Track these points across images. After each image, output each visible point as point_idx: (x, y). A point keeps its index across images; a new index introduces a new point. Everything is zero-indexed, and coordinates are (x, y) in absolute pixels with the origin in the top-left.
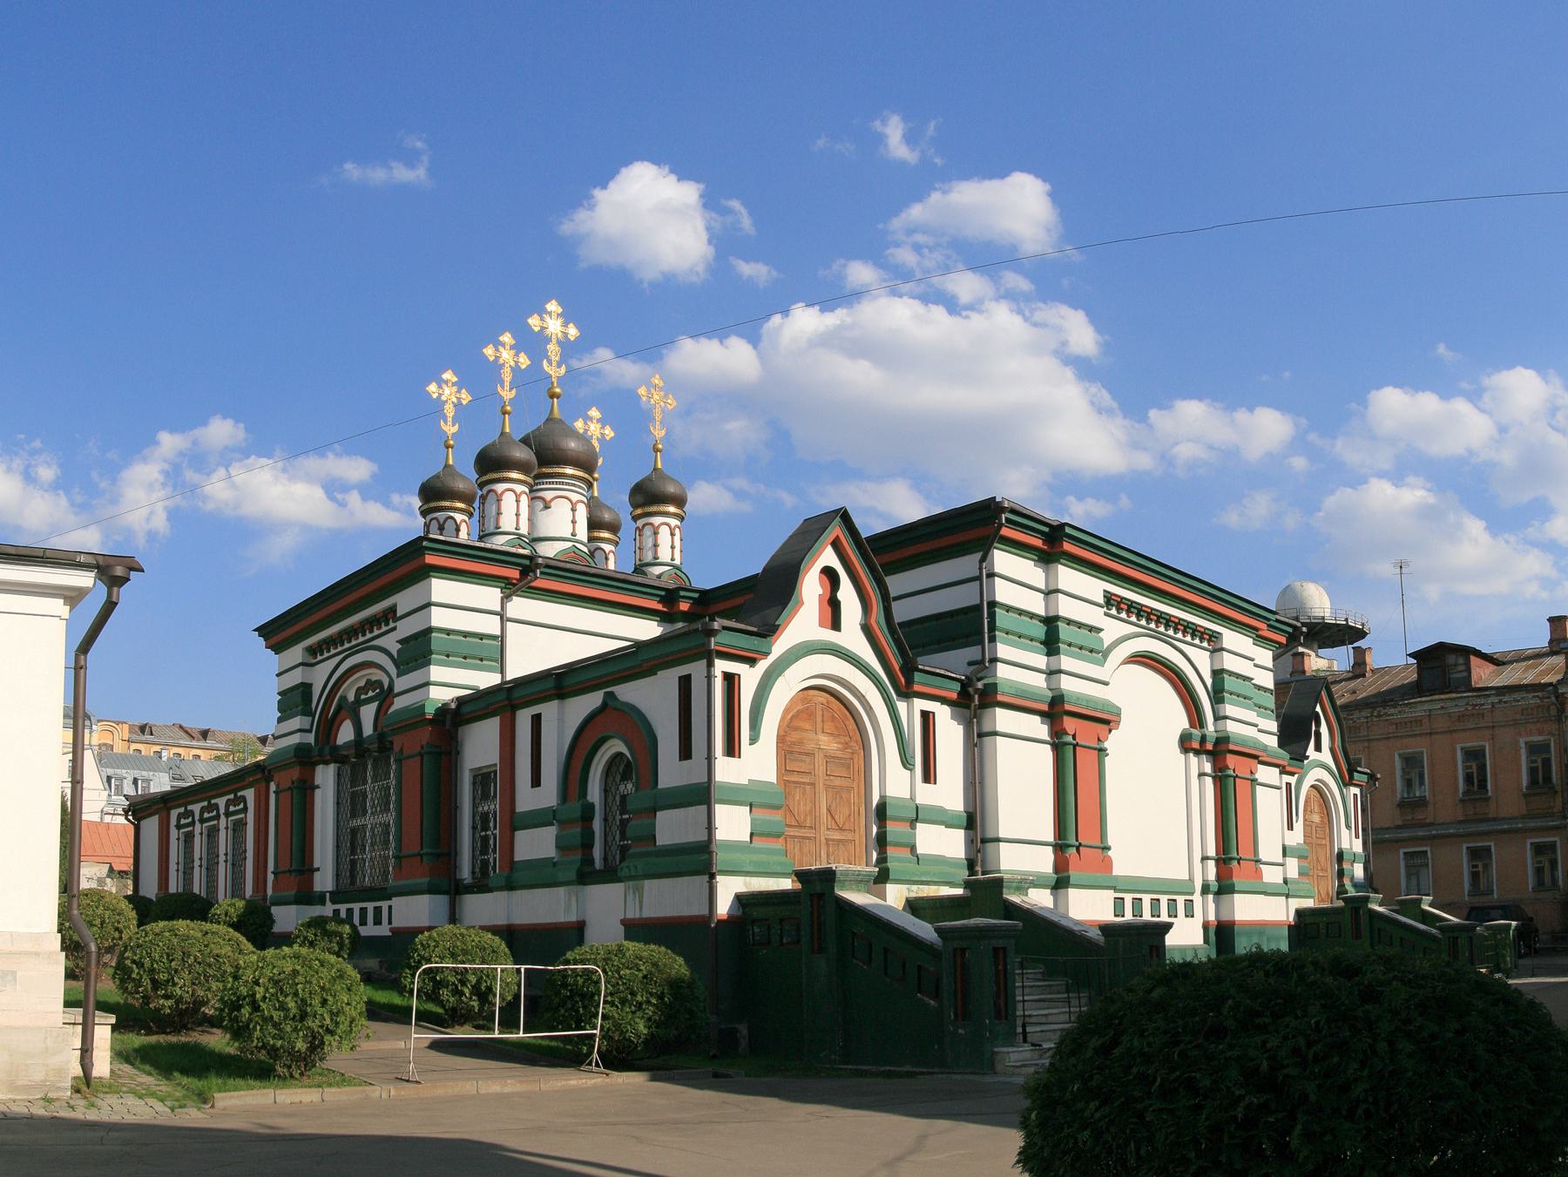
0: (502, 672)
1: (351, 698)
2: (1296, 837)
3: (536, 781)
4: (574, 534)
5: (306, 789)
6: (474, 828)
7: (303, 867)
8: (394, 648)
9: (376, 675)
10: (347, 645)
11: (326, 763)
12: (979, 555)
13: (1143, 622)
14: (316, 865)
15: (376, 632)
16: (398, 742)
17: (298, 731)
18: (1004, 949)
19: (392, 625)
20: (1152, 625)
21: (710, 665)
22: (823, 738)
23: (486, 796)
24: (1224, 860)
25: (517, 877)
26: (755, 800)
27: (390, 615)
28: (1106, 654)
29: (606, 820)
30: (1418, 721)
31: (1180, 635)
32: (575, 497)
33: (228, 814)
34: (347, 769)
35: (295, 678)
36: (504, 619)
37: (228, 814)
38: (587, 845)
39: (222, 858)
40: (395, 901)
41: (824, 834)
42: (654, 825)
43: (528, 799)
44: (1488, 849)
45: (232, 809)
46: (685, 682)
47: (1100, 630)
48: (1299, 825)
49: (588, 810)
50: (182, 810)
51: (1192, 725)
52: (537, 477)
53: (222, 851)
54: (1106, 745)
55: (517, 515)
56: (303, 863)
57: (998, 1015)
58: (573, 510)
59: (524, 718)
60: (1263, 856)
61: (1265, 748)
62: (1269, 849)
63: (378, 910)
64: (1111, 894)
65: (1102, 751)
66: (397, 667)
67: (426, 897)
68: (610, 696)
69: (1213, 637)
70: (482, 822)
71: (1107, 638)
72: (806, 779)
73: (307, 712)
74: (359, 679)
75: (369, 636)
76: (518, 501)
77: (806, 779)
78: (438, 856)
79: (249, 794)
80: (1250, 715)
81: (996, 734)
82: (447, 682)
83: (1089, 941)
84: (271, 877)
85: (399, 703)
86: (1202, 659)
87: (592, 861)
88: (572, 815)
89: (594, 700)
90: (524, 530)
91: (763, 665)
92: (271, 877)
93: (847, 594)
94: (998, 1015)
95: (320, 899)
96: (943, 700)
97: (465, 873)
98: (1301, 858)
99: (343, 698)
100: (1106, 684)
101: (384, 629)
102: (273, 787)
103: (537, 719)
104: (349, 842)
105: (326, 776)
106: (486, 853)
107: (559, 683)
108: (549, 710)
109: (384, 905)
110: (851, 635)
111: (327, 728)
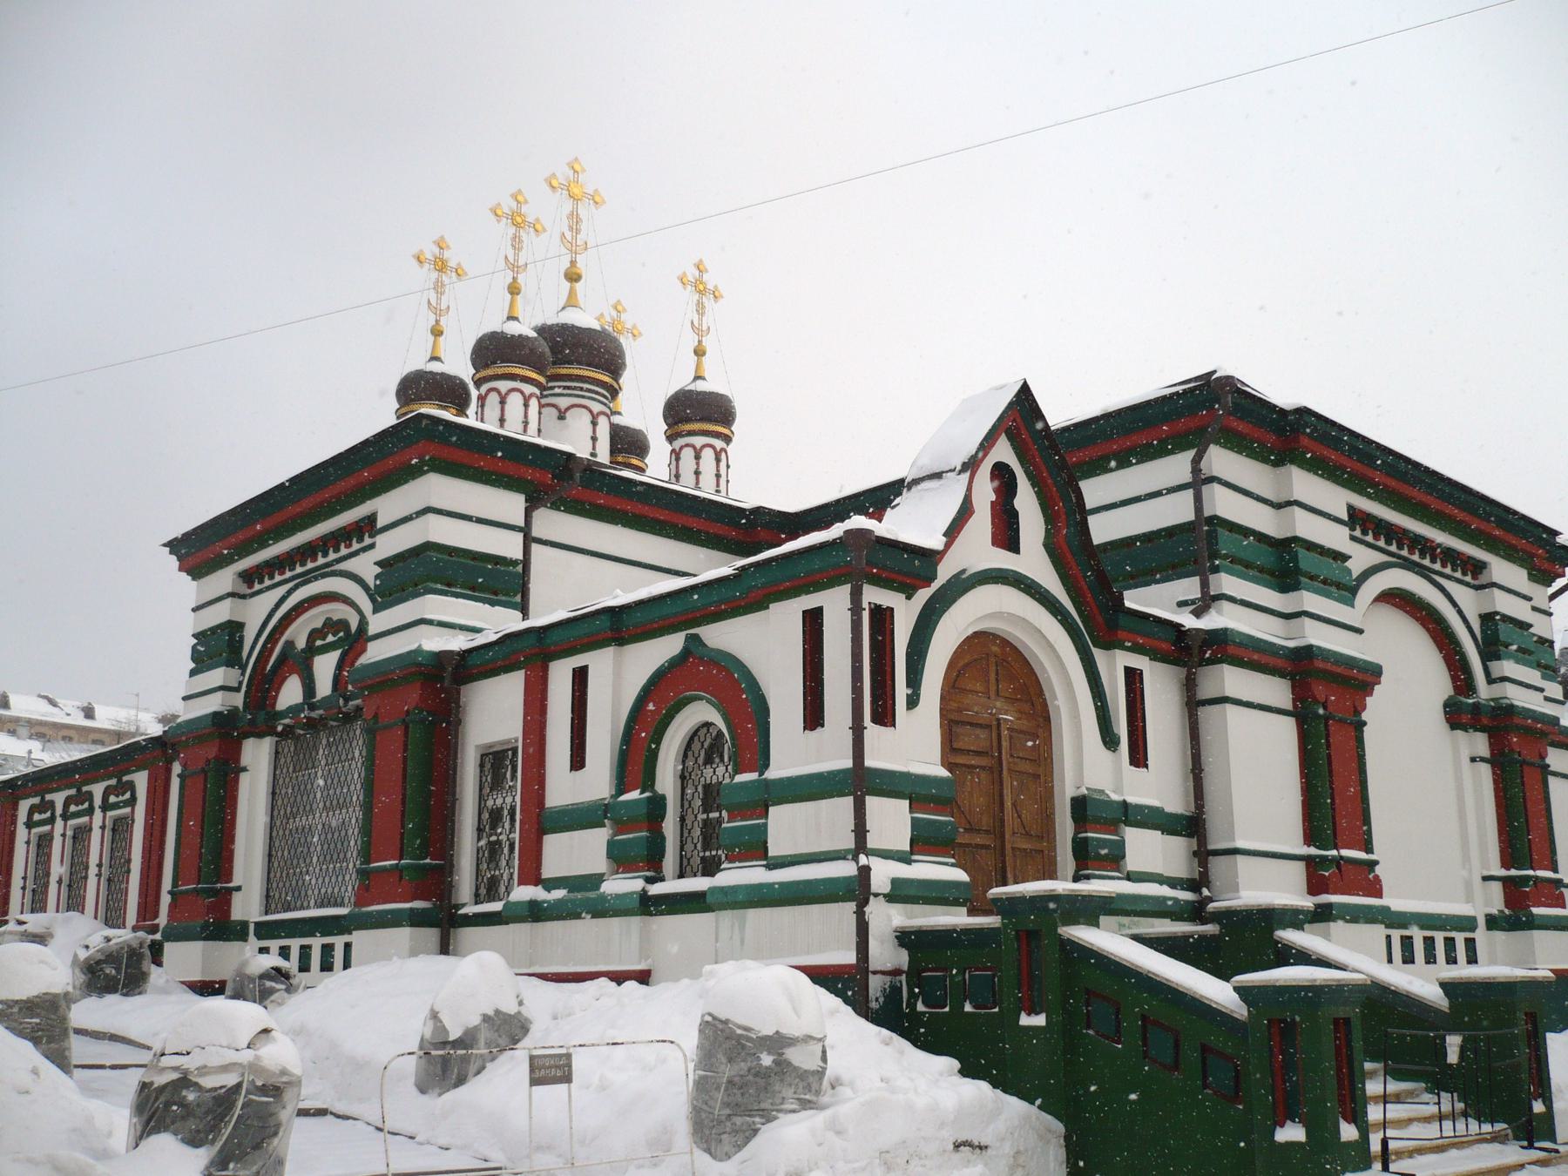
1: (301, 643)
3: (578, 760)
5: (227, 772)
6: (480, 830)
9: (338, 611)
10: (299, 570)
11: (260, 735)
12: (1191, 454)
13: (1393, 548)
15: (344, 551)
17: (217, 694)
27: (368, 526)
28: (1354, 591)
29: (683, 819)
32: (597, 407)
33: (106, 807)
35: (220, 614)
37: (106, 807)
39: (93, 870)
42: (765, 825)
43: (565, 787)
45: (112, 799)
46: (813, 619)
50: (36, 800)
52: (552, 378)
53: (93, 860)
58: (594, 424)
59: (560, 675)
63: (327, 950)
64: (1379, 931)
66: (373, 601)
68: (694, 640)
69: (1477, 567)
70: (491, 819)
71: (1356, 566)
74: (314, 618)
75: (332, 556)
76: (526, 405)
81: (1225, 700)
82: (452, 622)
83: (1437, 1011)
84: (165, 900)
85: (376, 652)
89: (669, 646)
91: (923, 595)
92: (165, 900)
93: (1026, 502)
99: (290, 644)
100: (1360, 631)
102: (177, 768)
103: (580, 676)
105: (257, 755)
107: (618, 626)
108: (600, 663)
109: (339, 941)
110: (1033, 560)
111: (263, 687)
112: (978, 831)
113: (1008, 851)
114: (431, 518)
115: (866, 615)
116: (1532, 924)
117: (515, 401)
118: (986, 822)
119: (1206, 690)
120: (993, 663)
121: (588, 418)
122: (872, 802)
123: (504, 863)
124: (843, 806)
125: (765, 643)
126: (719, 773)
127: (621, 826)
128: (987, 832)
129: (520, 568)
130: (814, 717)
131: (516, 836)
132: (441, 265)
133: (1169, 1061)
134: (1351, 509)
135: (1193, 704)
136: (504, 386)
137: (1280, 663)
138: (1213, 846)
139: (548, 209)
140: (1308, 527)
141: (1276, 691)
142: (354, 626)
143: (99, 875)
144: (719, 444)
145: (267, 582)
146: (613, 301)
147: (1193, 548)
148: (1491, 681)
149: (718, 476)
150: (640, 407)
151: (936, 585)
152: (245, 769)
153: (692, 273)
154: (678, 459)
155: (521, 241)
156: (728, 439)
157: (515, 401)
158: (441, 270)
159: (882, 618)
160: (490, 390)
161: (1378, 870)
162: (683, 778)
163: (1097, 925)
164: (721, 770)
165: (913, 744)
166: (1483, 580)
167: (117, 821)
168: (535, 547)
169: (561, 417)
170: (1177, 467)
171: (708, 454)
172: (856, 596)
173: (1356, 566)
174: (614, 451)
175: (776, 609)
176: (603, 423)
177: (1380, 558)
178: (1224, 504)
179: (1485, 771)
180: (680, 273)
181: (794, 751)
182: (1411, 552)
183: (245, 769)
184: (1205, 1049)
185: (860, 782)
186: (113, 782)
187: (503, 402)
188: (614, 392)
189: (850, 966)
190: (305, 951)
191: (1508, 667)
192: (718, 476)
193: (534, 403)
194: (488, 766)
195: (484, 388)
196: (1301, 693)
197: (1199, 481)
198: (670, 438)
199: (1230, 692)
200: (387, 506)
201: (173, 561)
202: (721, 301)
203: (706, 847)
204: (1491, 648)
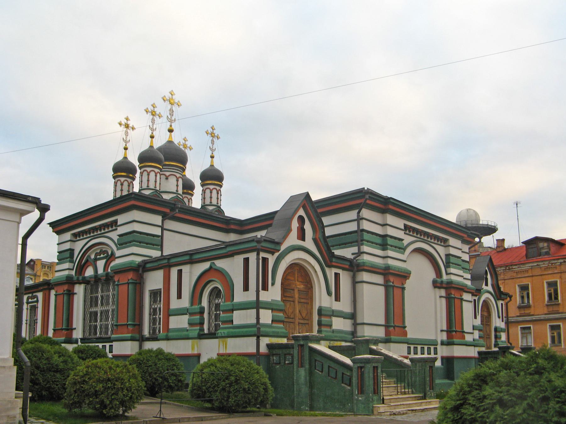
0: (162, 251)
1: (93, 257)
2: (478, 322)
3: (179, 296)
4: (177, 191)
5: (71, 294)
6: (150, 314)
7: (70, 329)
8: (116, 238)
9: (104, 248)
10: (92, 234)
11: (80, 283)
12: (357, 211)
13: (419, 236)
14: (74, 326)
15: (106, 230)
16: (116, 279)
17: (65, 270)
18: (377, 367)
19: (114, 228)
20: (422, 237)
21: (258, 254)
22: (298, 283)
23: (155, 301)
24: (449, 331)
26: (275, 307)
29: (209, 313)
30: (527, 271)
31: (432, 241)
32: (178, 175)
34: (89, 287)
35: (67, 246)
36: (163, 229)
38: (202, 324)
40: (114, 344)
41: (297, 321)
42: (233, 316)
43: (175, 304)
44: (560, 325)
45: (30, 300)
46: (246, 261)
47: (402, 240)
48: (479, 317)
49: (202, 309)
51: (437, 277)
54: (405, 286)
55: (156, 182)
57: (374, 393)
59: (174, 272)
60: (466, 330)
61: (466, 286)
62: (467, 328)
64: (406, 346)
65: (403, 289)
67: (130, 342)
70: (154, 312)
71: (405, 243)
72: (291, 299)
73: (72, 261)
74: (97, 249)
75: (103, 231)
76: (156, 176)
77: (291, 299)
78: (134, 325)
79: (40, 295)
80: (460, 272)
86: (441, 249)
87: (204, 330)
89: (206, 265)
90: (158, 188)
91: (277, 254)
93: (308, 226)
94: (374, 393)
96: (344, 269)
97: (146, 332)
98: (480, 330)
99: (89, 256)
100: (405, 261)
101: (110, 229)
103: (180, 272)
104: (91, 317)
105: (79, 290)
106: (156, 324)
107: (191, 258)
108: (186, 269)
110: (309, 243)
111: (81, 268)
114: (135, 224)
116: (453, 344)
117: (152, 175)
119: (359, 279)
121: (175, 179)
122: (261, 311)
123: (158, 324)
125: (233, 267)
130: (246, 288)
131: (162, 316)
132: (127, 126)
133: (334, 377)
134: (405, 226)
135: (355, 283)
136: (149, 169)
137: (381, 271)
138: (359, 321)
139: (163, 108)
140: (390, 231)
141: (379, 279)
142: (110, 253)
143: (26, 324)
144: (218, 188)
145: (81, 238)
146: (183, 137)
147: (357, 238)
148: (447, 274)
149: (218, 199)
150: (193, 172)
151: (280, 252)
152: (76, 294)
153: (210, 130)
154: (205, 193)
155: (154, 120)
157: (152, 175)
159: (265, 260)
160: (144, 171)
161: (406, 329)
162: (210, 302)
164: (220, 300)
165: (274, 294)
166: (447, 244)
167: (31, 307)
168: (165, 231)
169: (167, 178)
170: (353, 215)
171: (214, 192)
172: (258, 254)
173: (405, 243)
174: (184, 188)
175: (236, 257)
176: (180, 181)
177: (414, 239)
178: (366, 225)
179: (444, 301)
180: (206, 130)
181: (240, 296)
182: (424, 237)
183: (76, 294)
184: (322, 372)
185: (258, 305)
186: (30, 295)
187: (148, 175)
188: (184, 170)
189: (254, 353)
191: (452, 270)
192: (218, 199)
193: (158, 175)
194: (152, 296)
195: (142, 170)
196: (386, 281)
197: (359, 219)
199: (365, 280)
200: (121, 219)
201: (51, 229)
202: (219, 140)
204: (448, 265)
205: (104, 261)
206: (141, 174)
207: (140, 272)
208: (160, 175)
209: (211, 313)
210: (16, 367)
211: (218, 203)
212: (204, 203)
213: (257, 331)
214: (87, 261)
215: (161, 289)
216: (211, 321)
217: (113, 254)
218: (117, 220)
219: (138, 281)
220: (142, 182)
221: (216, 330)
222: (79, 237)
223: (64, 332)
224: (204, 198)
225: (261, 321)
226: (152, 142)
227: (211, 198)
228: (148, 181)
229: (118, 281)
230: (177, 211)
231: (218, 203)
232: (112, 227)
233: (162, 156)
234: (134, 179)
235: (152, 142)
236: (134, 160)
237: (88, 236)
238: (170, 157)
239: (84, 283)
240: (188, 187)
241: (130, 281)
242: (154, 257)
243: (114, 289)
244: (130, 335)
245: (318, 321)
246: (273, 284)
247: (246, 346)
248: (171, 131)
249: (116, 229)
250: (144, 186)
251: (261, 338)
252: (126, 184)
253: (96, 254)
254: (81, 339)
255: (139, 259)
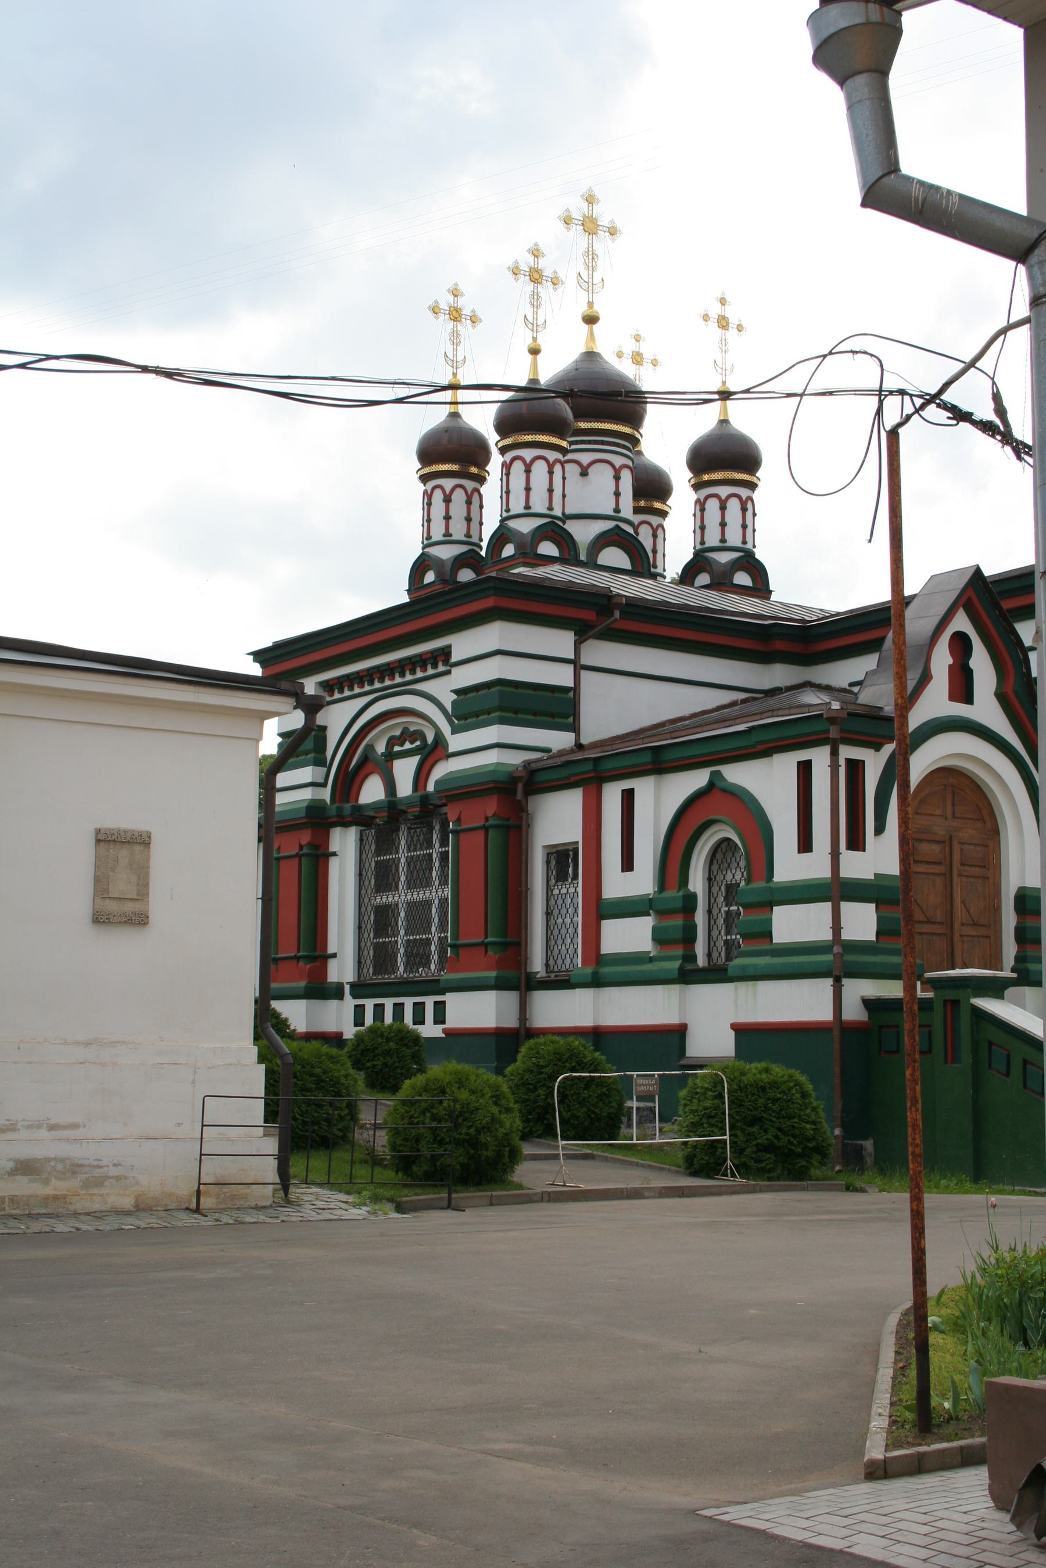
1: (381, 748)
3: (628, 864)
4: (617, 510)
8: (448, 700)
9: (415, 724)
10: (377, 685)
11: (345, 824)
14: (331, 950)
15: (419, 674)
16: (451, 812)
19: (441, 668)
21: (834, 753)
25: (604, 972)
32: (618, 461)
38: (689, 938)
40: (450, 998)
42: (770, 921)
43: (616, 885)
46: (805, 769)
49: (690, 900)
55: (551, 491)
56: (314, 948)
66: (451, 722)
67: (494, 992)
68: (716, 776)
73: (320, 761)
74: (394, 727)
75: (409, 677)
76: (551, 473)
78: (505, 945)
87: (693, 958)
88: (671, 907)
89: (697, 780)
93: (981, 663)
95: (336, 992)
97: (537, 965)
99: (370, 747)
101: (430, 671)
103: (628, 797)
104: (377, 921)
105: (345, 843)
107: (654, 753)
108: (644, 788)
110: (986, 709)
111: (348, 782)
112: (934, 923)
113: (957, 938)
115: (842, 771)
117: (540, 469)
118: (939, 916)
120: (956, 785)
121: (610, 472)
122: (846, 907)
124: (825, 909)
125: (768, 783)
126: (737, 875)
127: (662, 913)
128: (940, 923)
129: (571, 694)
130: (805, 844)
131: (580, 920)
136: (528, 454)
139: (564, 252)
142: (430, 738)
144: (744, 492)
149: (744, 527)
150: (666, 441)
152: (334, 854)
154: (703, 510)
156: (752, 486)
157: (540, 469)
158: (455, 320)
159: (855, 768)
162: (710, 880)
163: (1003, 998)
169: (584, 473)
171: (734, 505)
172: (834, 753)
174: (637, 494)
176: (626, 477)
181: (790, 866)
183: (334, 854)
185: (838, 891)
187: (528, 471)
190: (419, 1008)
192: (744, 527)
194: (553, 862)
198: (697, 487)
203: (728, 933)
205: (415, 760)
206: (507, 467)
207: (519, 796)
208: (562, 464)
209: (715, 911)
210: (263, 1066)
211: (744, 542)
212: (702, 543)
213: (838, 961)
214: (365, 759)
215: (577, 843)
216: (715, 933)
217: (440, 741)
218: (449, 647)
219: (511, 823)
220: (508, 492)
221: (728, 958)
222: (341, 691)
223: (305, 966)
224: (703, 528)
225: (845, 936)
226: (535, 364)
227: (723, 525)
228: (528, 489)
229: (459, 819)
230: (617, 614)
231: (744, 542)
232: (435, 666)
233: (564, 407)
234: (481, 480)
235: (535, 364)
236: (482, 419)
237: (367, 688)
238: (593, 407)
239: (357, 824)
240: (652, 489)
241: (491, 822)
242: (554, 751)
243: (444, 842)
244: (494, 974)
245: (1016, 928)
246: (879, 829)
247: (805, 1002)
248: (591, 320)
249: (449, 672)
250: (517, 507)
251: (844, 981)
252: (459, 496)
253: (392, 742)
254: (353, 985)
255: (516, 759)
